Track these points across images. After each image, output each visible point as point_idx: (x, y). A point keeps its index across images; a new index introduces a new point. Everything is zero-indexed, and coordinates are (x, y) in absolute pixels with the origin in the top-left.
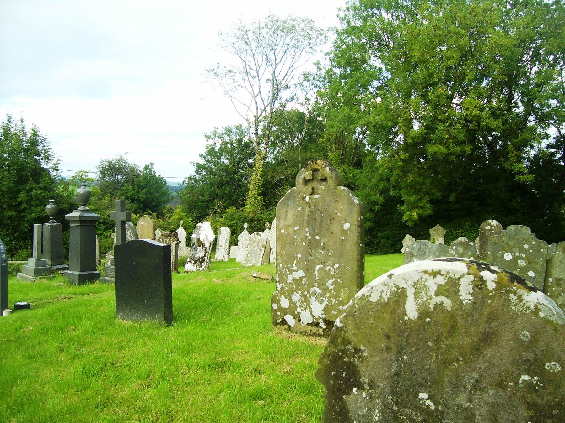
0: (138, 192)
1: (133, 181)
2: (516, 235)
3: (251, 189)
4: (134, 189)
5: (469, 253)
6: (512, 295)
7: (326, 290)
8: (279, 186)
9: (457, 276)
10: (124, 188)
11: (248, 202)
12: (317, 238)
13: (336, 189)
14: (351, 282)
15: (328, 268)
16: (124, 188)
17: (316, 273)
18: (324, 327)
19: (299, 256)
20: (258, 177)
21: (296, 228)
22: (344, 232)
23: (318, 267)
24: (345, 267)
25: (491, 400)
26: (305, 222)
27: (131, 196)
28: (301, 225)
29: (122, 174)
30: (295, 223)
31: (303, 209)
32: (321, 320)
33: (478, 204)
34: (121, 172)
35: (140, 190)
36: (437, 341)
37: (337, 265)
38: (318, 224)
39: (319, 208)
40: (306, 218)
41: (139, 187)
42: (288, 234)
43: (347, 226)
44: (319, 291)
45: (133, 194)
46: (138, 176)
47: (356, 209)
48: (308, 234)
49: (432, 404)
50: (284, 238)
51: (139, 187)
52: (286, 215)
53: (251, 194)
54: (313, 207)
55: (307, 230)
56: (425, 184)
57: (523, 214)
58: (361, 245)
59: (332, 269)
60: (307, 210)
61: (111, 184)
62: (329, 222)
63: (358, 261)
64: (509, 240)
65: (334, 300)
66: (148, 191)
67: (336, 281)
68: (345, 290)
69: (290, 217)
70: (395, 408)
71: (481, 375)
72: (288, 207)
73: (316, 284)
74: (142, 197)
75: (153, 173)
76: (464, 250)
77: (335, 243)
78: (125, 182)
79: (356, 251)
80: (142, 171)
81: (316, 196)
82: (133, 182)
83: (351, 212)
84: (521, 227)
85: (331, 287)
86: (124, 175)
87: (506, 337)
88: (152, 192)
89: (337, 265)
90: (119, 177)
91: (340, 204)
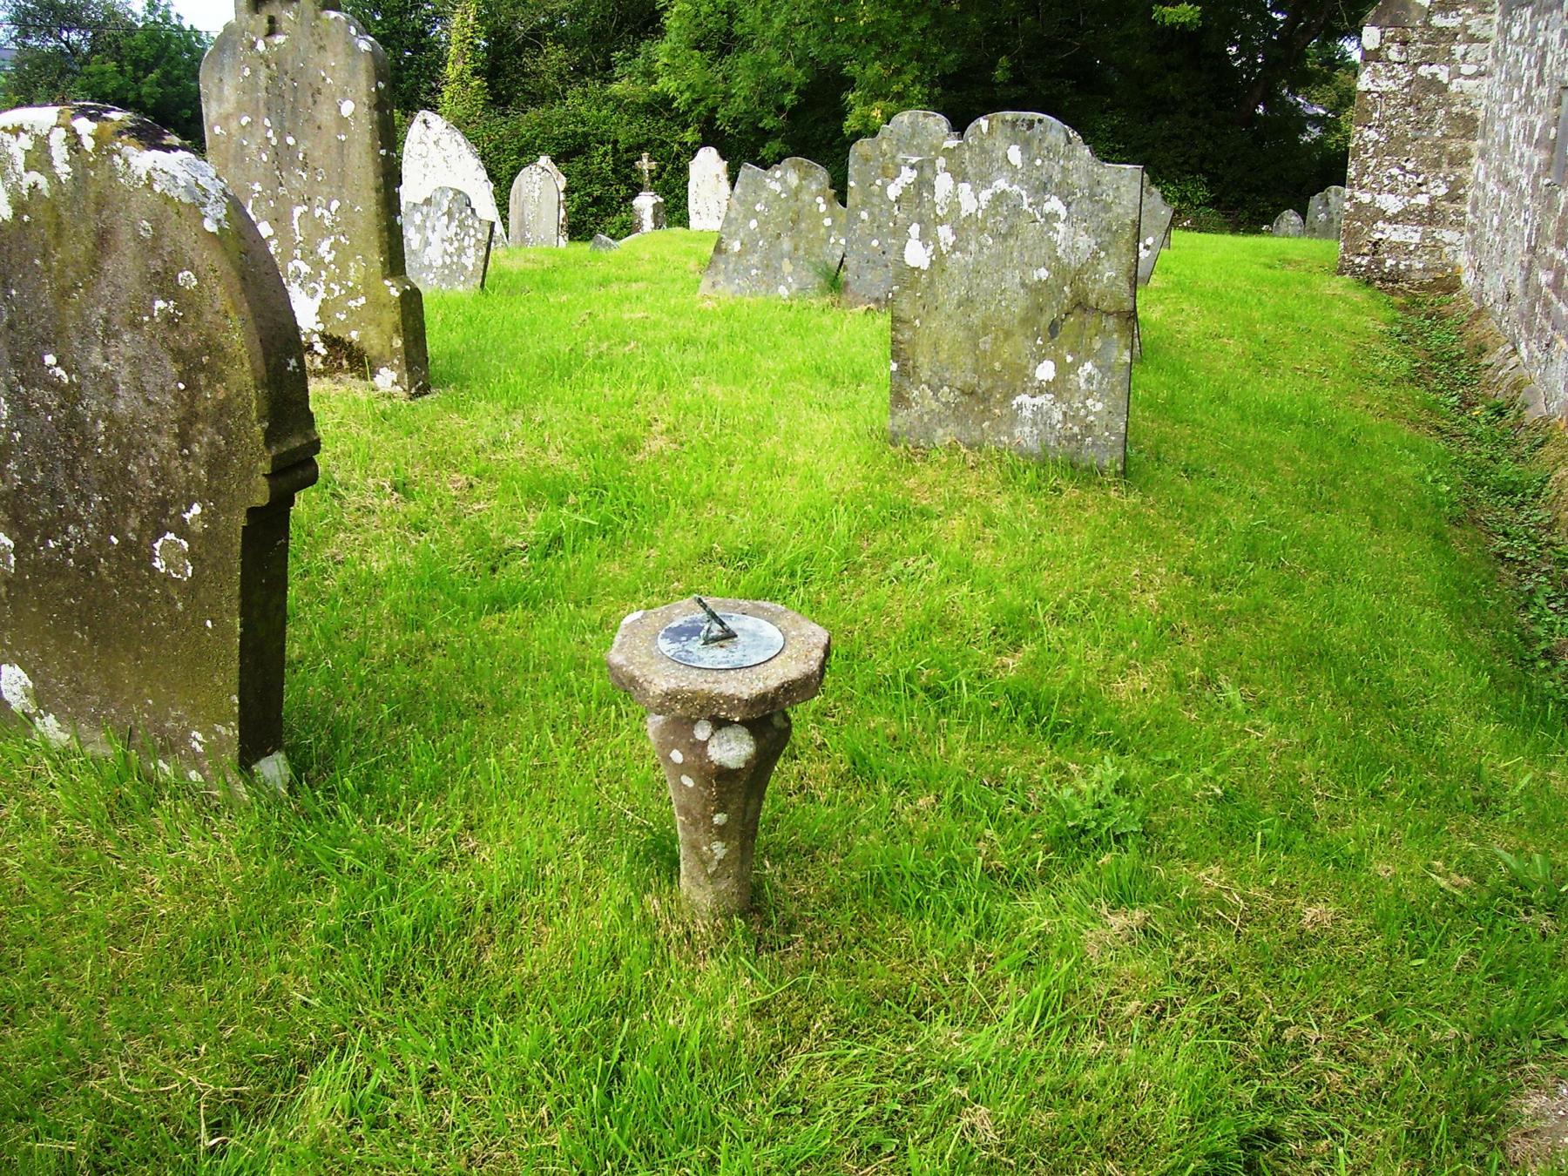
0: (136, 80)
1: (119, 48)
2: (913, 136)
3: (452, 58)
4: (122, 72)
5: (814, 187)
6: (116, 158)
7: (318, 264)
8: (531, 45)
9: (45, 132)
10: (93, 68)
11: (447, 95)
12: (291, 141)
13: (318, 17)
14: (368, 241)
15: (318, 213)
16: (93, 68)
17: (296, 226)
18: (324, 352)
19: (257, 187)
20: (471, 21)
21: (245, 120)
22: (342, 122)
23: (298, 211)
24: (352, 208)
25: (130, 353)
26: (261, 104)
27: (114, 93)
28: (254, 113)
29: (78, 24)
30: (241, 109)
31: (254, 72)
32: (316, 338)
33: (1072, 86)
34: (78, 21)
35: (141, 74)
36: (45, 256)
37: (335, 205)
38: (288, 107)
39: (288, 67)
40: (262, 94)
41: (136, 63)
42: (229, 134)
43: (347, 108)
44: (305, 268)
45: (120, 87)
46: (130, 30)
47: (363, 65)
48: (270, 134)
49: (63, 373)
50: (223, 147)
51: (136, 63)
52: (221, 90)
53: (451, 71)
54: (273, 66)
55: (267, 122)
56: (907, 30)
57: (1194, 114)
58: (383, 152)
59: (326, 213)
60: (263, 73)
61: (44, 61)
62: (310, 100)
63: (377, 191)
64: (899, 150)
65: (337, 288)
66: (166, 74)
67: (337, 241)
68: (356, 262)
69: (229, 91)
70: (22, 390)
71: (109, 310)
72: (222, 69)
73: (298, 252)
74: (150, 95)
75: (175, 21)
76: (801, 179)
77: (326, 152)
78: (94, 51)
79: (371, 168)
80: (141, 14)
81: (279, 39)
82: (116, 51)
83: (353, 73)
84: (926, 116)
85: (329, 258)
86: (86, 27)
87: (125, 234)
88: (179, 78)
89: (335, 205)
90: (74, 37)
91: (330, 54)
